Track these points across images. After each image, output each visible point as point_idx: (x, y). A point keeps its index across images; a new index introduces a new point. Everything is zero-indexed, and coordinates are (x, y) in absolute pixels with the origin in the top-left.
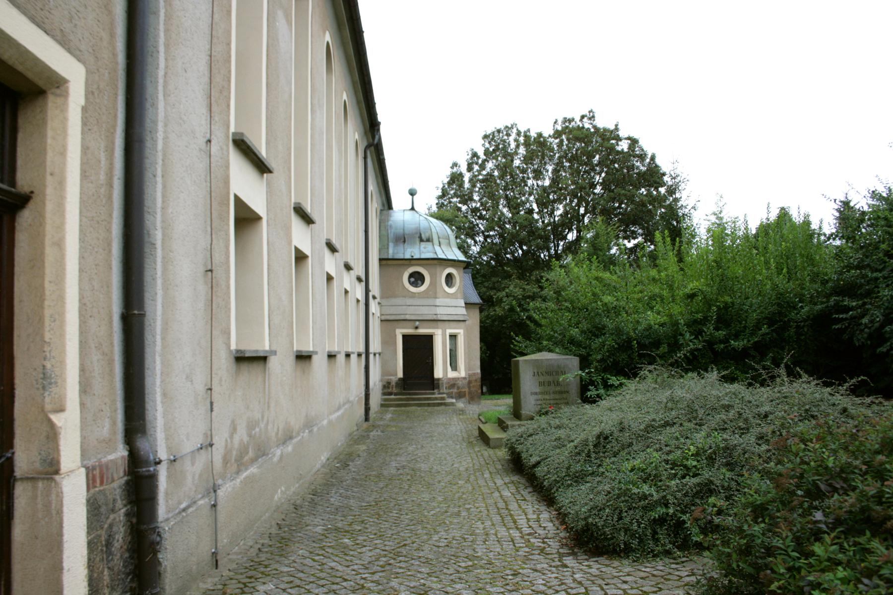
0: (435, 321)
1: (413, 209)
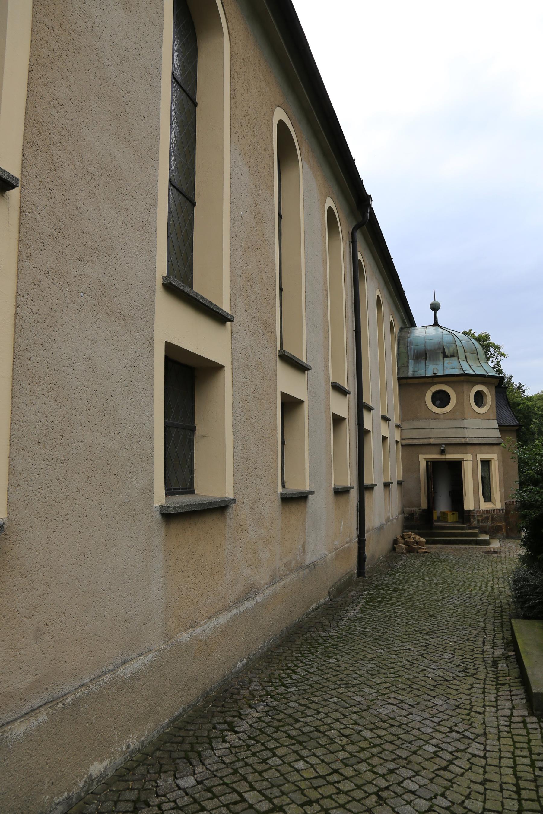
0: (464, 446)
1: (436, 324)
